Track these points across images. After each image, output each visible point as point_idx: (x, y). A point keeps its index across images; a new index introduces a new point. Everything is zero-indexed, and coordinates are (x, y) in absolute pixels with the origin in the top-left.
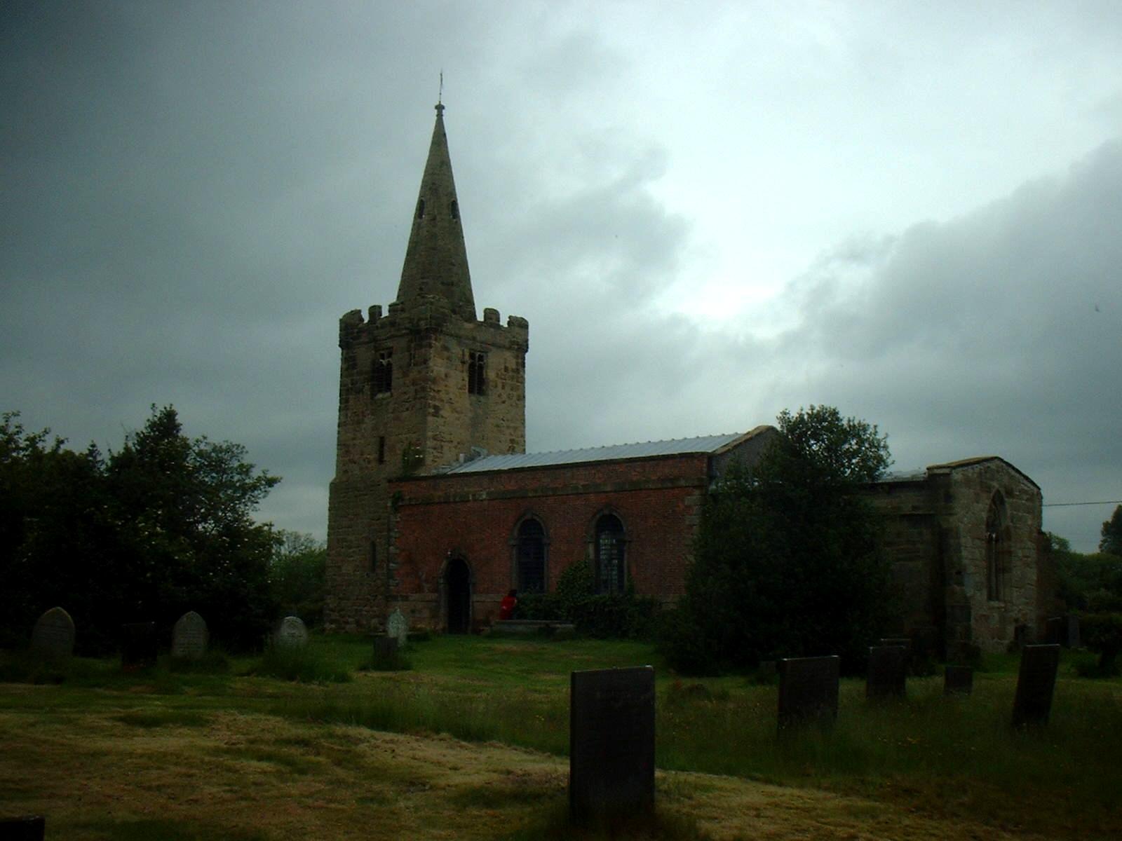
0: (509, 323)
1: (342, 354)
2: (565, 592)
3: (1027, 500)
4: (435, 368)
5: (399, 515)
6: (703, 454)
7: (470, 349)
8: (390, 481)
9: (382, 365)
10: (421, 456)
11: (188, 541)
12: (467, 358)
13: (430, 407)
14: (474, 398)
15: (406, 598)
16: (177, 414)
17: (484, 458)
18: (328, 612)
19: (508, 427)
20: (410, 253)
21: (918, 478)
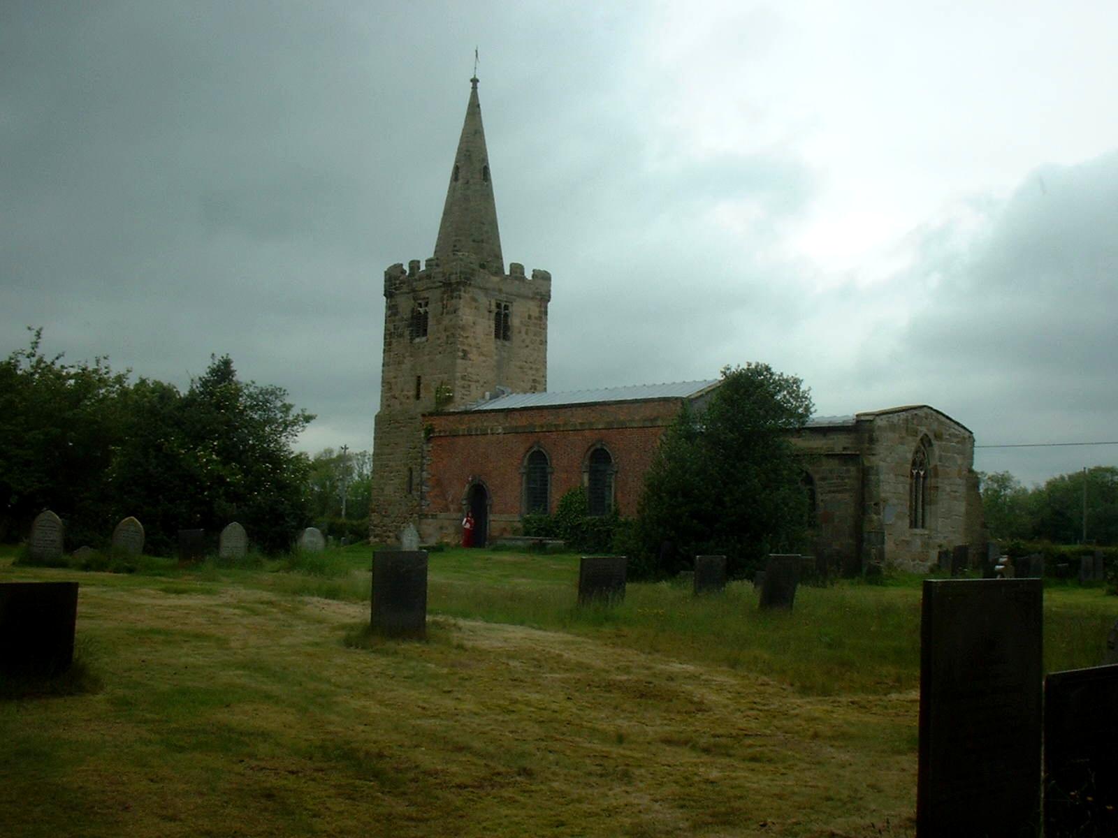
0: (533, 277)
1: (387, 302)
2: (564, 513)
3: (958, 442)
4: (465, 317)
5: (431, 445)
6: (677, 398)
7: (496, 300)
8: (423, 415)
9: (420, 313)
10: (451, 394)
11: (238, 466)
12: (493, 307)
13: (458, 351)
14: (499, 343)
15: (434, 517)
16: (232, 362)
17: (508, 396)
18: (372, 527)
19: (531, 368)
20: (447, 213)
21: (848, 423)
